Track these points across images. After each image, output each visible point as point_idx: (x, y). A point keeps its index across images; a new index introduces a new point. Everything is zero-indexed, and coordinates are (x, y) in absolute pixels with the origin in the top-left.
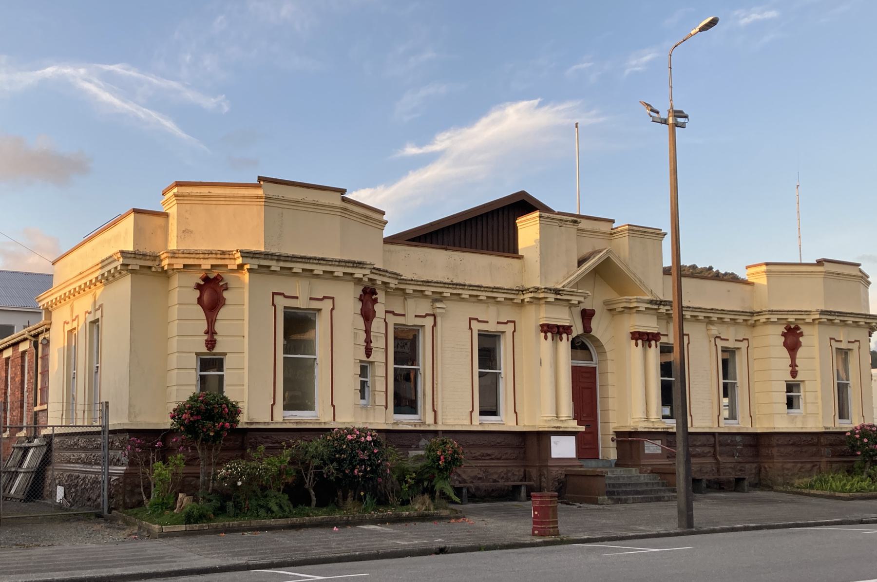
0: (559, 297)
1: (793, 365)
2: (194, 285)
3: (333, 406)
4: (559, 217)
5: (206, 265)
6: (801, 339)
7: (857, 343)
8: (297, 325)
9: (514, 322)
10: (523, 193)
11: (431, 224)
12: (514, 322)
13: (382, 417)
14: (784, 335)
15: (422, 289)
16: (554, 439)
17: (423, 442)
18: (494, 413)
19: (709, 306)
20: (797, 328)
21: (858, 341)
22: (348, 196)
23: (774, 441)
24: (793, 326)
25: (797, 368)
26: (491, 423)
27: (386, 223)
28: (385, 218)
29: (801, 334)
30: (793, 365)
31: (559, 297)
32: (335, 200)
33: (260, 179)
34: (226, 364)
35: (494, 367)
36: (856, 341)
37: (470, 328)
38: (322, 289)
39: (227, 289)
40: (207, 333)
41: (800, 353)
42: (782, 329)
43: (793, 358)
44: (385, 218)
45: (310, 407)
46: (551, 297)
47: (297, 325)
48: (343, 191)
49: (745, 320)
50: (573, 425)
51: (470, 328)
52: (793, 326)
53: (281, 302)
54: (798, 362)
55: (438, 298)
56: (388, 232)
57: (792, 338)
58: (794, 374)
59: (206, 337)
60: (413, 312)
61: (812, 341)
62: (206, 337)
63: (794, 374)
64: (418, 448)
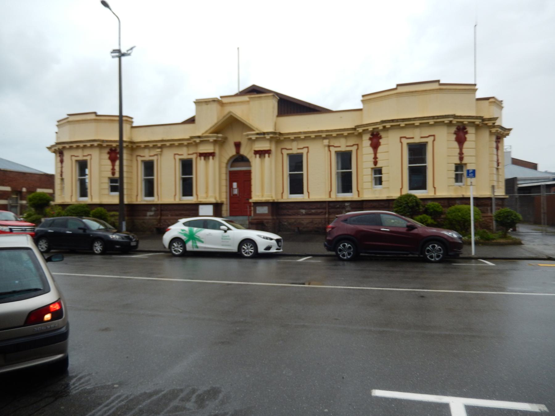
1: (375, 158)
3: (435, 188)
5: (370, 129)
7: (432, 138)
8: (83, 166)
10: (254, 86)
12: (308, 147)
14: (455, 133)
15: (297, 137)
17: (153, 209)
19: (146, 140)
21: (90, 155)
22: (441, 82)
24: (375, 133)
26: (86, 200)
27: (476, 90)
28: (477, 87)
29: (380, 138)
30: (375, 158)
32: (436, 86)
34: (383, 172)
35: (410, 167)
36: (89, 155)
38: (87, 152)
41: (380, 149)
42: (107, 150)
43: (375, 153)
44: (477, 87)
45: (302, 192)
46: (198, 140)
47: (83, 166)
48: (438, 81)
52: (461, 127)
55: (161, 147)
56: (479, 95)
58: (461, 159)
63: (461, 159)
64: (151, 211)
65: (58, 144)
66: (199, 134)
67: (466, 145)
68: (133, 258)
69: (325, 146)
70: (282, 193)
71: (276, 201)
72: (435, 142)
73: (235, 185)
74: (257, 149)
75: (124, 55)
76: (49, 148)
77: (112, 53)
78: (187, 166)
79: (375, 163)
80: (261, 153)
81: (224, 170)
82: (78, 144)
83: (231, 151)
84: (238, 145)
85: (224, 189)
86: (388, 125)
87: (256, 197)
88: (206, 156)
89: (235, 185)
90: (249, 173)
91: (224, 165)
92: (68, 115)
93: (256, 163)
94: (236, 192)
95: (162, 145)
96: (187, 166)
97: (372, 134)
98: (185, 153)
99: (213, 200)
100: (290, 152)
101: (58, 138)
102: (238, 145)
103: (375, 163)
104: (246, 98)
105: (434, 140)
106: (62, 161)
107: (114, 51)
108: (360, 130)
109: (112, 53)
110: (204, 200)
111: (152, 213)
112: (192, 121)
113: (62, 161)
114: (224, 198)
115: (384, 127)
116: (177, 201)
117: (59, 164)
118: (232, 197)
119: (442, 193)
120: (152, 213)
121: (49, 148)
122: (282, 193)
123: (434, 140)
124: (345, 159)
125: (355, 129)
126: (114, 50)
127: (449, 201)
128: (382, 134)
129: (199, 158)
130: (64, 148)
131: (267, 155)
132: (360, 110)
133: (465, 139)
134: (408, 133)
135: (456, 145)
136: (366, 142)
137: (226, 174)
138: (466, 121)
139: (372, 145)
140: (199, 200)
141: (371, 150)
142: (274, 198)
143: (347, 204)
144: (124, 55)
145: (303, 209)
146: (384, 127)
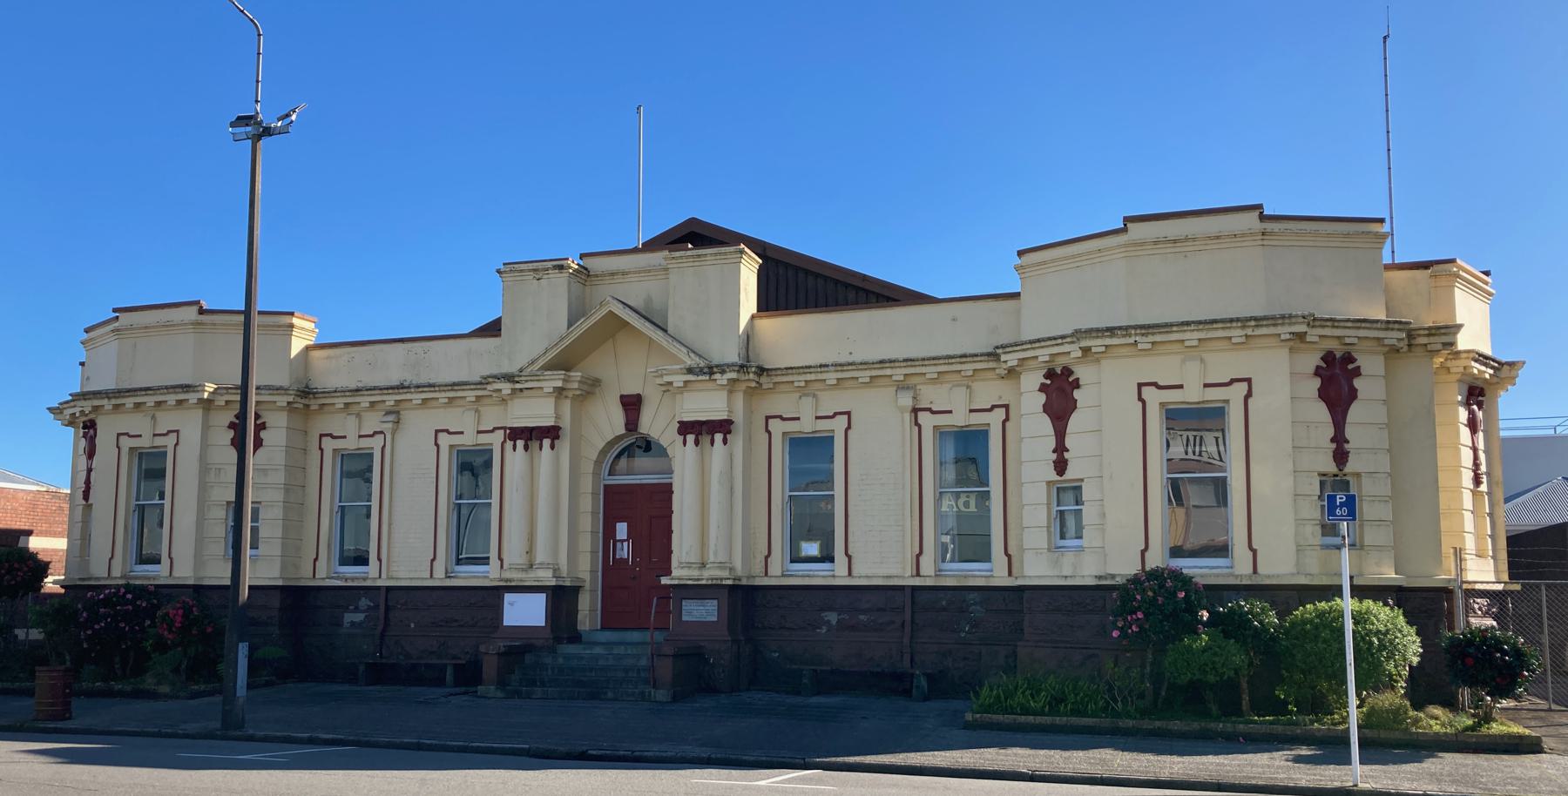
0: (518, 386)
1: (1339, 439)
2: (1312, 369)
4: (531, 266)
5: (1044, 354)
6: (1357, 383)
9: (767, 418)
11: (864, 278)
13: (219, 574)
14: (1318, 372)
15: (809, 377)
16: (508, 597)
18: (362, 560)
20: (1348, 358)
23: (1027, 595)
25: (1066, 455)
30: (1339, 439)
31: (518, 386)
33: (1127, 220)
37: (437, 445)
39: (1078, 387)
40: (1332, 440)
41: (1075, 423)
43: (1060, 435)
46: (506, 388)
49: (373, 404)
50: (248, 580)
51: (437, 445)
53: (127, 443)
54: (1349, 432)
57: (1060, 394)
58: (1341, 456)
59: (1054, 456)
60: (349, 431)
61: (1106, 394)
62: (1054, 456)
63: (1341, 456)
64: (357, 610)
65: (76, 397)
66: (512, 368)
67: (1355, 413)
68: (759, 788)
69: (902, 410)
70: (918, 556)
71: (744, 582)
72: (1250, 401)
73: (622, 529)
74: (689, 417)
75: (268, 132)
76: (56, 411)
77: (233, 125)
78: (473, 467)
79: (1061, 466)
80: (696, 430)
81: (587, 484)
82: (97, 403)
83: (609, 421)
84: (632, 405)
85: (585, 543)
86: (1096, 344)
87: (681, 571)
88: (529, 436)
89: (622, 529)
90: (665, 491)
91: (588, 467)
92: (115, 310)
93: (684, 458)
94: (624, 551)
95: (396, 399)
96: (473, 467)
97: (1050, 374)
98: (469, 426)
99: (546, 577)
100: (791, 427)
101: (86, 379)
102: (632, 405)
103: (1061, 466)
104: (658, 258)
105: (1249, 395)
106: (91, 453)
107: (243, 120)
108: (1011, 359)
109: (233, 125)
110: (517, 577)
111: (359, 617)
112: (492, 329)
113: (91, 453)
114: (585, 569)
115: (1086, 351)
116: (439, 579)
117: (83, 462)
118: (612, 570)
119: (1279, 567)
120: (359, 617)
121: (56, 411)
122: (918, 556)
123: (1249, 395)
124: (968, 452)
125: (993, 356)
126: (239, 118)
127: (1286, 596)
128: (1082, 372)
129: (509, 444)
130: (96, 409)
131: (546, 442)
132: (1016, 296)
133: (1353, 395)
134: (1163, 368)
135: (1321, 412)
136: (1030, 400)
137: (594, 494)
138: (1351, 335)
139: (1323, 394)
140: (507, 575)
141: (1046, 425)
142: (739, 571)
143: (972, 596)
144: (268, 132)
145: (831, 609)
146: (1086, 351)
